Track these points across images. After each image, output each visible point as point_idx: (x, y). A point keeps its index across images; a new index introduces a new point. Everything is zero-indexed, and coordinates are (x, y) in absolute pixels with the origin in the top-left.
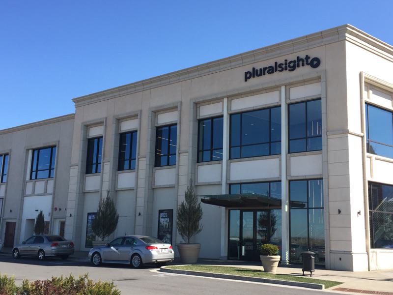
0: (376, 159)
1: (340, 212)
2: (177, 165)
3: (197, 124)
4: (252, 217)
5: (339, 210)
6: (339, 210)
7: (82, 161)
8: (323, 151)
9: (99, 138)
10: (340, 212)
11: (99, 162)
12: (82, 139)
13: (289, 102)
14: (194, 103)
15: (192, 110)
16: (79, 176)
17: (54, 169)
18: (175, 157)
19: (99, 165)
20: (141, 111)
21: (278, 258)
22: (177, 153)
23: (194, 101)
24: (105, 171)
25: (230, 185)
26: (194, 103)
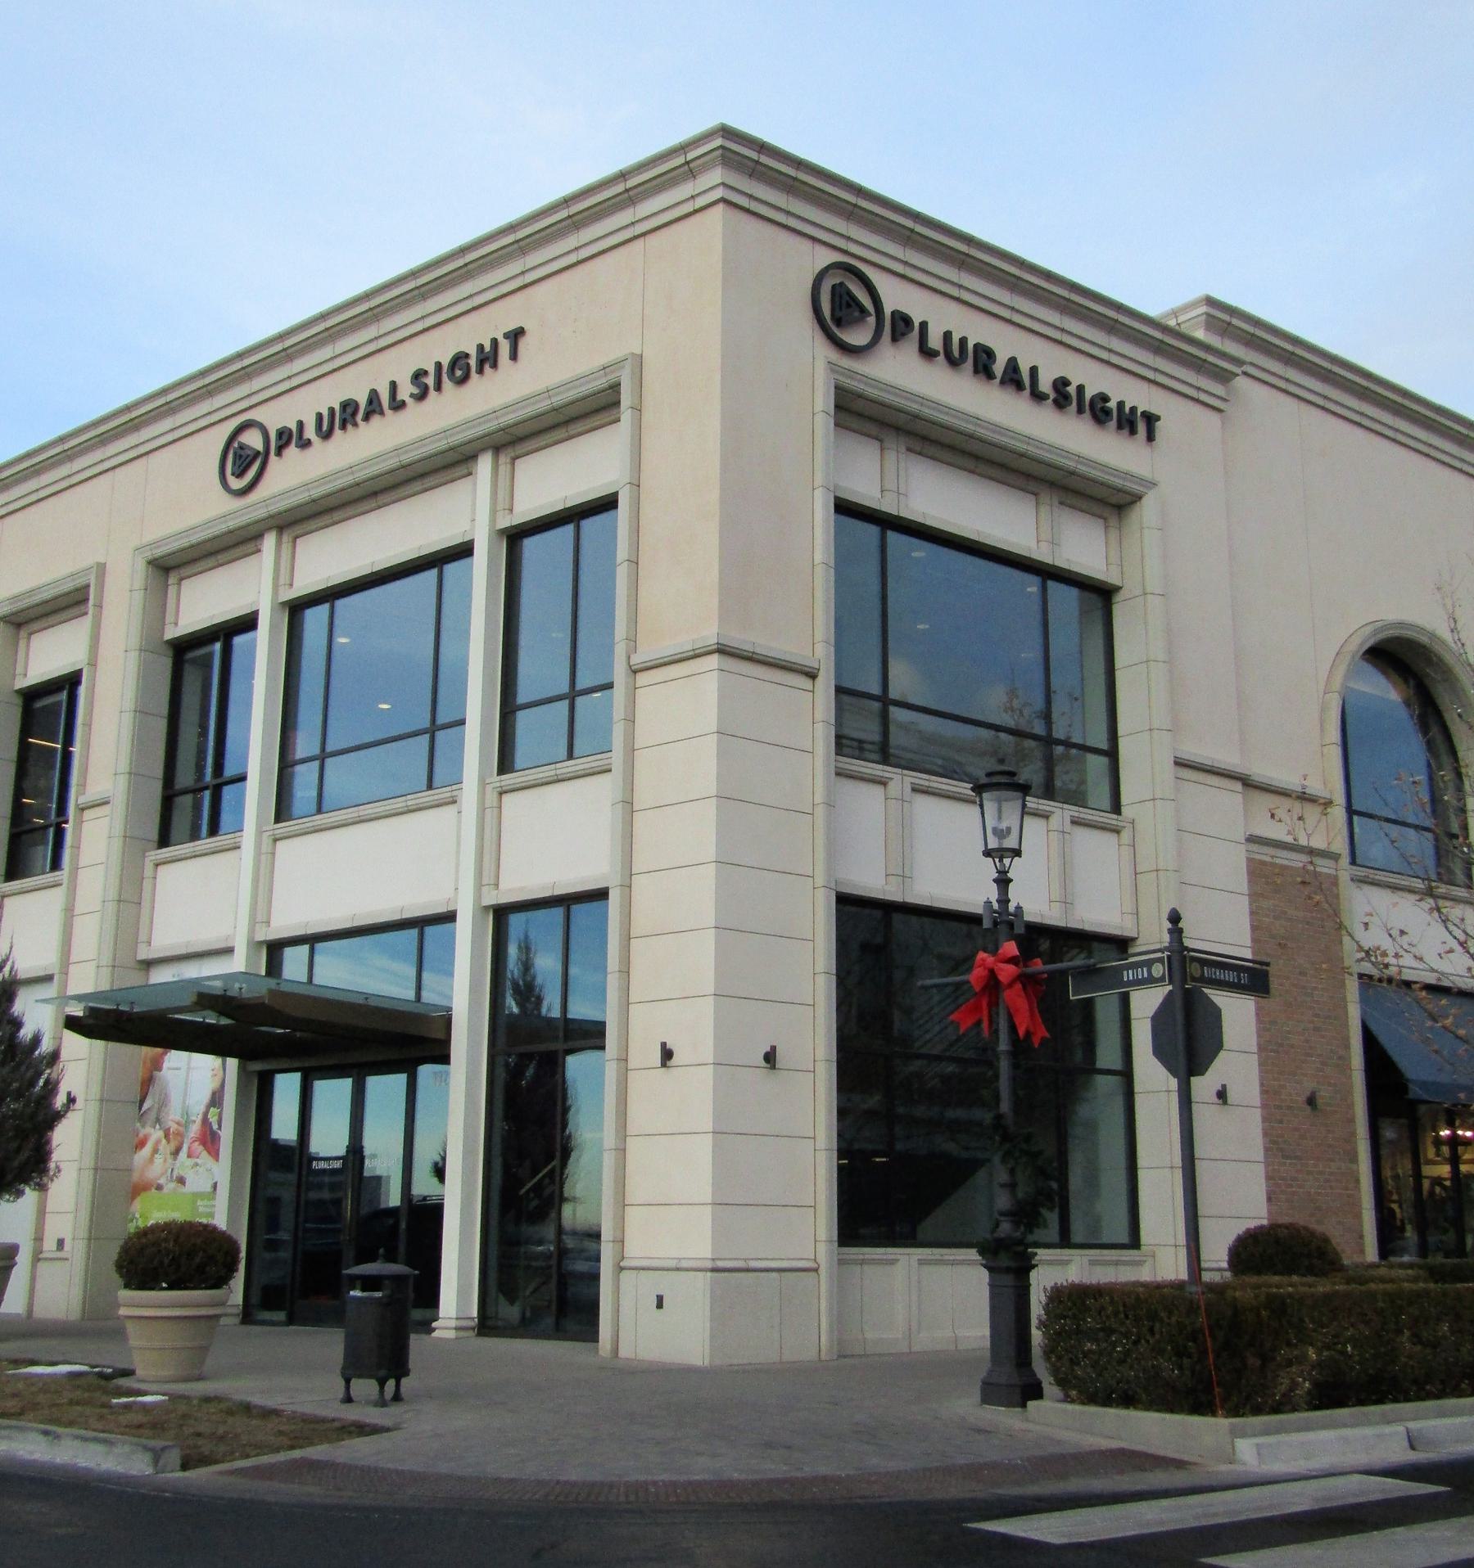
0: (914, 790)
1: (667, 1054)
2: (617, 758)
3: (166, 663)
4: (1114, 1068)
5: (664, 1045)
6: (664, 1045)
7: (134, 774)
8: (245, 833)
9: (71, 682)
10: (667, 1054)
11: (230, 771)
12: (135, 641)
13: (505, 522)
14: (150, 563)
15: (139, 596)
16: (115, 870)
17: (242, 778)
18: (611, 698)
19: (228, 792)
20: (639, 359)
21: (163, 1245)
22: (620, 676)
23: (149, 555)
24: (84, 860)
25: (501, 914)
26: (150, 563)
